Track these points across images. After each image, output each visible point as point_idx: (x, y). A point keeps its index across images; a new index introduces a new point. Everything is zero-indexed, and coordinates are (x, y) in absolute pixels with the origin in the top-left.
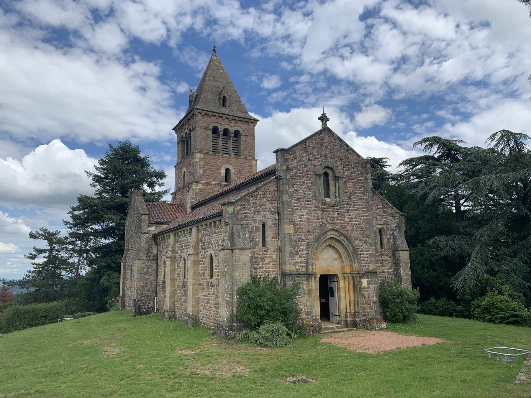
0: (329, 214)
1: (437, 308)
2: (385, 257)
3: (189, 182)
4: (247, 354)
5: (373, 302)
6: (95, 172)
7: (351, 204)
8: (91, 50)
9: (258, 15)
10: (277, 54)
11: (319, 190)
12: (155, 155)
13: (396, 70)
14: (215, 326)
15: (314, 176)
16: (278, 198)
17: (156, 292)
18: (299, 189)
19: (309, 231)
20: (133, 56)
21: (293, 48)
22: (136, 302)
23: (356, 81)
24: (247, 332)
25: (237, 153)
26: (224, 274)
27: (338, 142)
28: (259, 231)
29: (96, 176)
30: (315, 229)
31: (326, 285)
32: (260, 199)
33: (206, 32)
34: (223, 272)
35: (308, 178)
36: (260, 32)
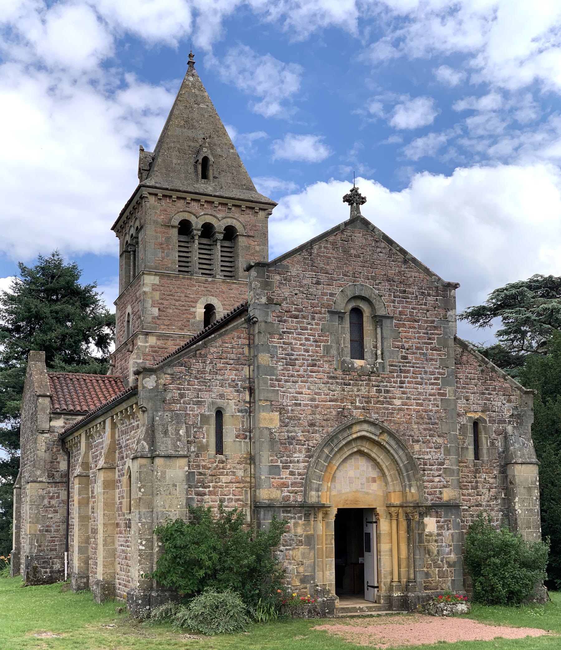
0: (359, 390)
5: (448, 563)
7: (408, 371)
8: (39, 66)
10: (429, 49)
11: (338, 343)
15: (327, 315)
16: (251, 361)
18: (294, 342)
20: (123, 74)
21: (465, 33)
30: (326, 420)
31: (353, 528)
35: (313, 319)
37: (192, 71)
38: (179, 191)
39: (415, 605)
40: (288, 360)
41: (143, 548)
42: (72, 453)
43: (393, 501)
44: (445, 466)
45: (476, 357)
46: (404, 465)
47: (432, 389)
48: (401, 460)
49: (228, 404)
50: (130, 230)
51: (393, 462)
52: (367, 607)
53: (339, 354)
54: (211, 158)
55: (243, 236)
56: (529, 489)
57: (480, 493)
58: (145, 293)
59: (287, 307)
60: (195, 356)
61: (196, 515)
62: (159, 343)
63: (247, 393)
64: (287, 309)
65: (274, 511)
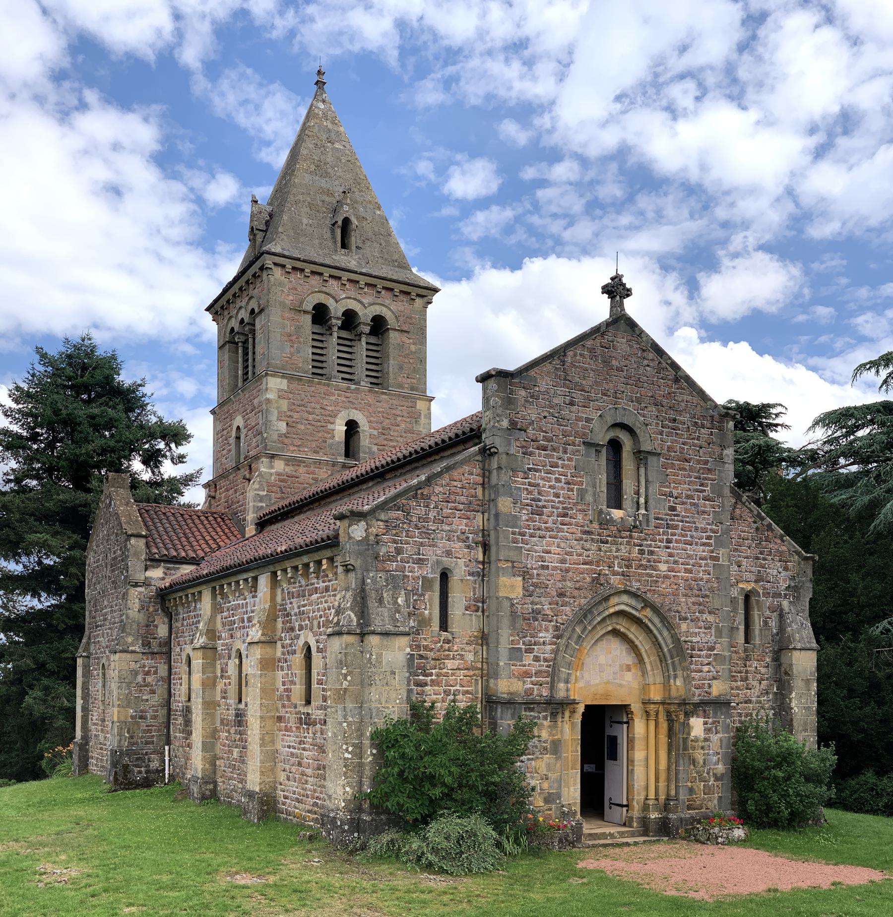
0: (618, 550)
2: (755, 664)
3: (252, 453)
4: (394, 889)
5: (715, 775)
7: (676, 527)
10: (489, 97)
11: (594, 486)
12: (154, 378)
13: (820, 153)
14: (316, 820)
15: (582, 448)
16: (486, 506)
17: (168, 735)
18: (541, 482)
19: (561, 595)
22: (116, 757)
23: (707, 183)
24: (396, 836)
25: (378, 380)
26: (341, 695)
30: (579, 589)
31: (601, 730)
32: (436, 507)
33: (283, 24)
34: (338, 691)
35: (565, 452)
36: (442, 29)
37: (322, 94)
38: (315, 263)
39: (677, 829)
40: (535, 508)
41: (350, 756)
42: (177, 614)
43: (652, 696)
44: (715, 652)
45: (751, 511)
46: (669, 650)
47: (704, 551)
48: (666, 643)
49: (456, 564)
50: (237, 313)
51: (655, 645)
52: (619, 832)
53: (595, 501)
54: (354, 220)
55: (395, 330)
57: (750, 686)
58: (268, 401)
59: (534, 434)
60: (415, 497)
61: (419, 712)
62: (288, 469)
63: (480, 549)
64: (534, 438)
65: (515, 709)
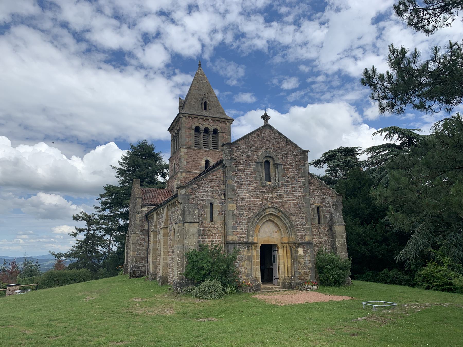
0: (269, 194)
1: (389, 277)
6: (119, 166)
7: (289, 187)
8: (141, 67)
9: (280, 27)
11: (260, 175)
15: (255, 164)
16: (224, 182)
19: (250, 209)
21: (310, 52)
27: (277, 135)
28: (207, 208)
29: (120, 169)
31: (267, 253)
33: (235, 45)
35: (250, 165)
36: (281, 41)
54: (208, 102)
56: (342, 236)
58: (181, 155)
60: (201, 181)
61: (202, 247)
